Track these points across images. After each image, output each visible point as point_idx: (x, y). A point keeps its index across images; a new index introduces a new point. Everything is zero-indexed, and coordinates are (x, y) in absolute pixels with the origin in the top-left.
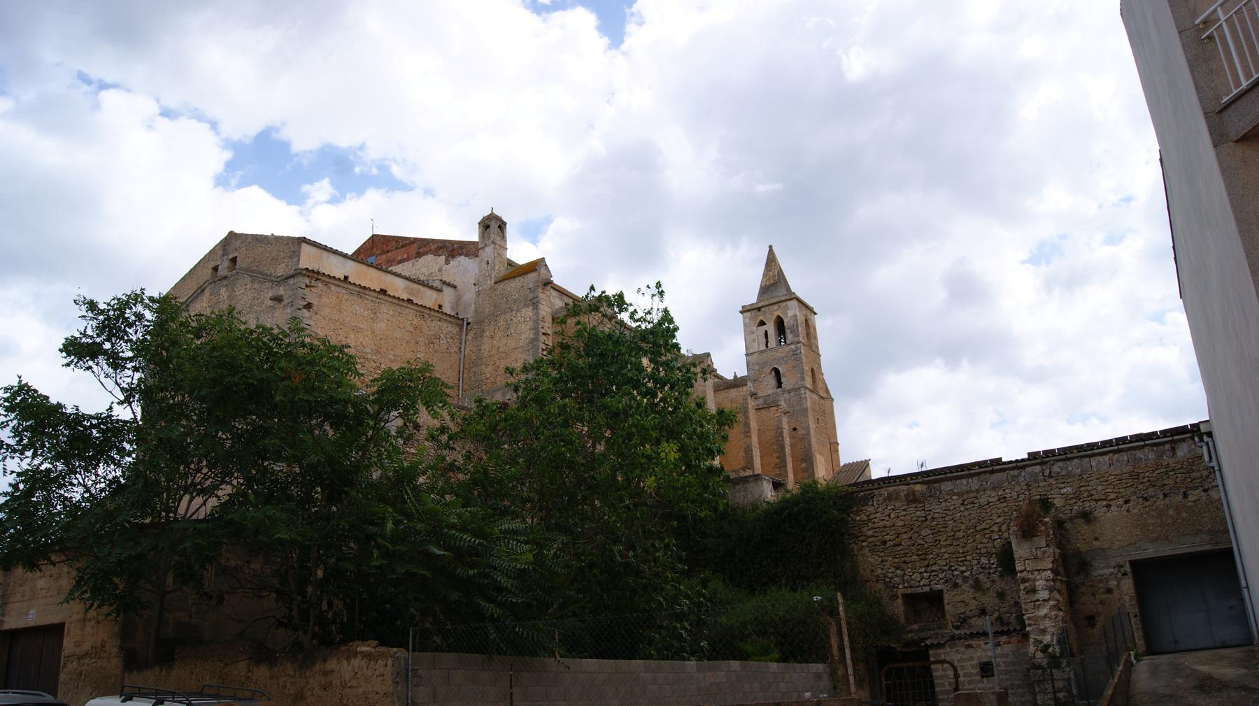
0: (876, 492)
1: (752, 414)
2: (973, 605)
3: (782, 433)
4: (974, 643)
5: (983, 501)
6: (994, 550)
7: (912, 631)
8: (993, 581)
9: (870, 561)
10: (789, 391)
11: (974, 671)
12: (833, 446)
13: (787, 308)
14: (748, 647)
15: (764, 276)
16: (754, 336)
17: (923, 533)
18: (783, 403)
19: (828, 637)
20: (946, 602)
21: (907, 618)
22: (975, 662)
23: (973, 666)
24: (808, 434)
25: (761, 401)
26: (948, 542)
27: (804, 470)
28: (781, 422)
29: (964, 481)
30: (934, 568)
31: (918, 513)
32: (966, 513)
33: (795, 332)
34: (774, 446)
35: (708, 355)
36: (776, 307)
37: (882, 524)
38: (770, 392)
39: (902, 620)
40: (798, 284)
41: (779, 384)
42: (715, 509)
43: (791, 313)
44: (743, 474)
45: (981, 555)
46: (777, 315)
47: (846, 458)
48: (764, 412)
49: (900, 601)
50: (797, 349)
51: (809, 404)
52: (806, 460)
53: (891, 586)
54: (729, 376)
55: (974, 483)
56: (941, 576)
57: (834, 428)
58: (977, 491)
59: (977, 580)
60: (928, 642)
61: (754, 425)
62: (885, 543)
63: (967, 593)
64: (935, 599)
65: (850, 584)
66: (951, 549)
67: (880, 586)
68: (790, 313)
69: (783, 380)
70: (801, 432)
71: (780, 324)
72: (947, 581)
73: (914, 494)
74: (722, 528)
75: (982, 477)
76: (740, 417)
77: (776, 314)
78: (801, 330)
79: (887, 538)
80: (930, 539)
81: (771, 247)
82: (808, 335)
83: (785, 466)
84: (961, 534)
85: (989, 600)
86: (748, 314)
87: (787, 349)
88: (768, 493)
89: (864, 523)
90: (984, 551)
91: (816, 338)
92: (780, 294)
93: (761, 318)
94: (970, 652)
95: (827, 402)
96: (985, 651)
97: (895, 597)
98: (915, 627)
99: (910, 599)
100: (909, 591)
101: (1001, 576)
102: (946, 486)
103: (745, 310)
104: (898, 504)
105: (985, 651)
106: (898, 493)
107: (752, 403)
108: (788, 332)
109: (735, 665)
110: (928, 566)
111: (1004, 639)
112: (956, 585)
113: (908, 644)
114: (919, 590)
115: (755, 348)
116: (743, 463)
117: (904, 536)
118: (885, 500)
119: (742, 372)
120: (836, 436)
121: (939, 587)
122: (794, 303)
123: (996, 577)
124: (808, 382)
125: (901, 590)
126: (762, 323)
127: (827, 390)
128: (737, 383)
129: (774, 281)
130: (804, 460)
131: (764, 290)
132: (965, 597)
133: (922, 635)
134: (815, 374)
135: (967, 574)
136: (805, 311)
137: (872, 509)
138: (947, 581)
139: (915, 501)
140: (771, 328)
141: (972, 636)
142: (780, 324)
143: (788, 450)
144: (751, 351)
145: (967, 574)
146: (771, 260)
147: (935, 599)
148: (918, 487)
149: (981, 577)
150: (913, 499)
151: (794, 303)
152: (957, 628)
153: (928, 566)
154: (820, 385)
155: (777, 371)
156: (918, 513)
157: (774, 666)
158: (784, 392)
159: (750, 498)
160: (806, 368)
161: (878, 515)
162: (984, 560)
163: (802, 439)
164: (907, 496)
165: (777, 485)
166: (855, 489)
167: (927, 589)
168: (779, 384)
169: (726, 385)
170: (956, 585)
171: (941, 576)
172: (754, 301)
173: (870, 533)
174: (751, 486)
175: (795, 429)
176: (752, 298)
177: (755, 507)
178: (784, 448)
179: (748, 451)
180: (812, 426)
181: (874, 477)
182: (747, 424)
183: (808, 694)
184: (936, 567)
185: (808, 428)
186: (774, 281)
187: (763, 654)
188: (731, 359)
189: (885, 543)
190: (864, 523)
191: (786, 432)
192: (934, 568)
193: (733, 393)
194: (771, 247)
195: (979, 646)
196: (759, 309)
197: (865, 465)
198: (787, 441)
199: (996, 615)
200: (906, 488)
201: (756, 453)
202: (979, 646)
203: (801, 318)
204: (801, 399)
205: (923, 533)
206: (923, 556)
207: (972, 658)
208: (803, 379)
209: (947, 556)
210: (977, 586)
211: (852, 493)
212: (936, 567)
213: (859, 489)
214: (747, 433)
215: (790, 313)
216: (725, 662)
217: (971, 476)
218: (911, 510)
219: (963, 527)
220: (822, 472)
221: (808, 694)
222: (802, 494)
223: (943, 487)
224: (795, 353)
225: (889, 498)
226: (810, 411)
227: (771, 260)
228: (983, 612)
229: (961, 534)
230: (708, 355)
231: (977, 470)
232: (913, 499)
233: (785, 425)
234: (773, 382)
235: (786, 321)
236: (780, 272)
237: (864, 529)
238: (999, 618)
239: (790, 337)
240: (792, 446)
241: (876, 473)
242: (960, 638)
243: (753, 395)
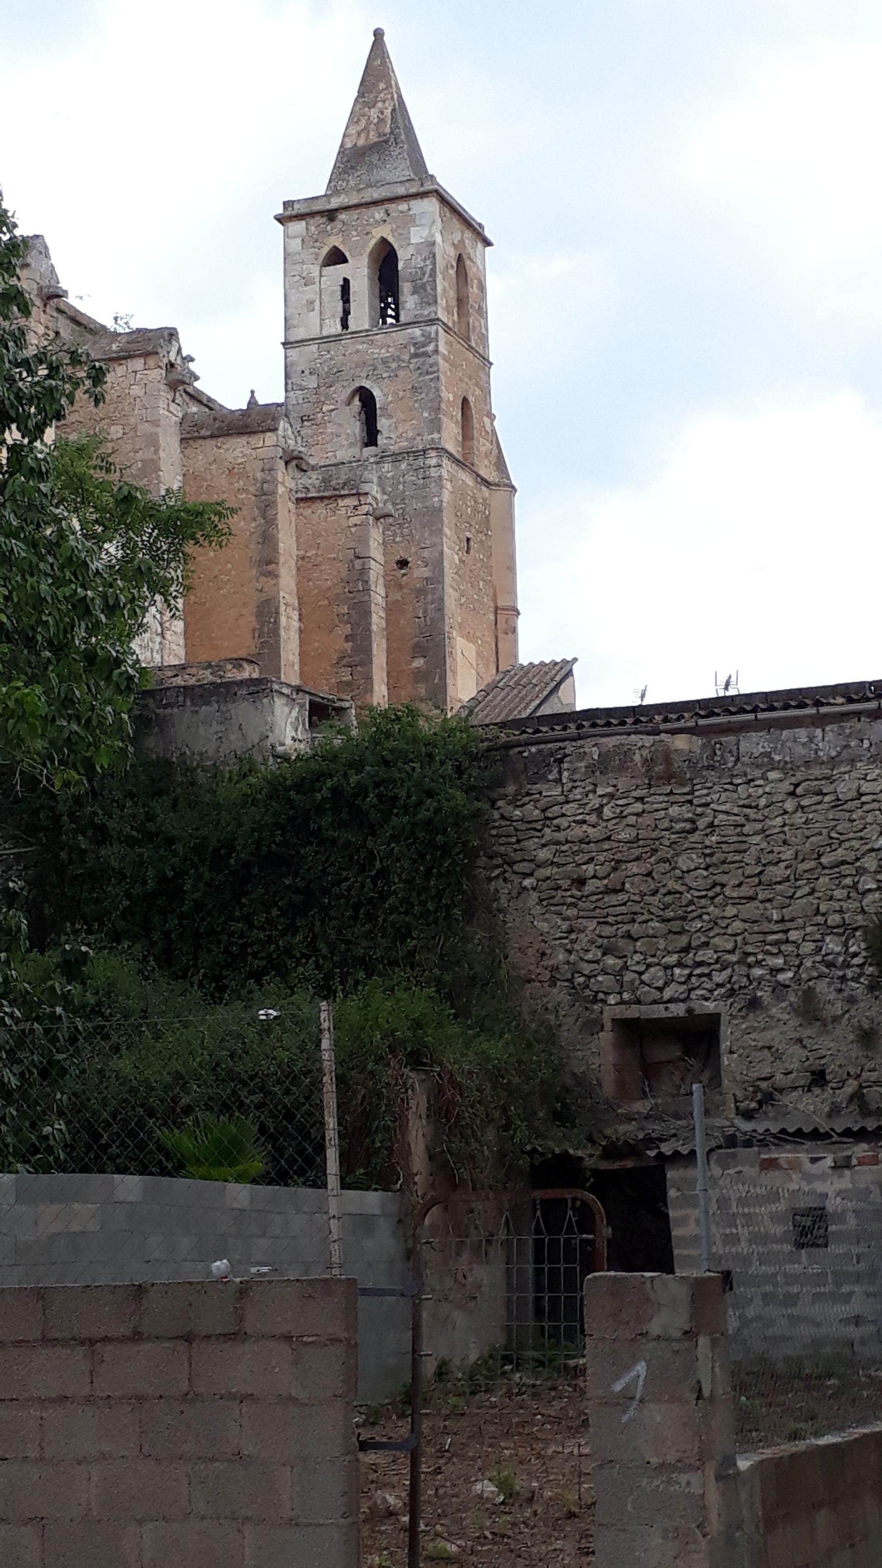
0: (569, 747)
1: (285, 511)
2: (794, 1058)
3: (364, 570)
4: (783, 1155)
5: (845, 788)
6: (860, 920)
7: (629, 1118)
8: (852, 1000)
9: (535, 929)
10: (397, 457)
11: (778, 1230)
12: (503, 618)
13: (409, 220)
14: (182, 1140)
15: (354, 119)
16: (311, 292)
17: (683, 863)
18: (374, 489)
19: (401, 1119)
20: (725, 1045)
21: (621, 1085)
22: (781, 1207)
23: (775, 1218)
24: (437, 579)
25: (313, 479)
26: (745, 891)
27: (420, 676)
28: (364, 540)
29: (802, 734)
30: (701, 956)
31: (674, 811)
32: (799, 818)
33: (425, 290)
34: (343, 607)
35: (171, 334)
36: (378, 213)
37: (578, 832)
38: (342, 455)
39: (608, 1088)
40: (449, 151)
41: (371, 436)
42: (89, 767)
43: (420, 234)
44: (232, 674)
45: (829, 929)
46: (382, 238)
47: (533, 647)
48: (320, 509)
49: (606, 1037)
50: (429, 339)
51: (446, 496)
52: (427, 649)
53: (587, 998)
54: (233, 400)
55: (827, 741)
56: (719, 977)
57: (511, 569)
58: (834, 762)
59: (809, 995)
60: (667, 1149)
61: (287, 543)
62: (581, 882)
63: (780, 1023)
64: (698, 1037)
65: (474, 988)
66: (751, 910)
67: (559, 994)
68: (417, 236)
69: (382, 423)
70: (419, 572)
71: (386, 262)
72: (732, 993)
73: (668, 761)
74: (151, 817)
75: (849, 726)
76: (242, 525)
77: (378, 233)
78: (444, 285)
79: (590, 869)
80: (699, 880)
81: (378, 34)
82: (461, 302)
83: (367, 661)
84: (778, 872)
85: (836, 1048)
86: (299, 227)
87: (401, 336)
88: (287, 728)
89: (532, 827)
90: (834, 919)
91: (482, 312)
92: (394, 174)
93: (336, 241)
94: (771, 1179)
95: (501, 494)
96: (808, 1178)
97: (593, 1026)
98: (641, 1107)
99: (633, 1032)
100: (633, 1012)
101: (871, 988)
102: (754, 744)
103: (290, 215)
104: (624, 782)
105: (808, 1178)
106: (627, 754)
107: (286, 482)
108: (406, 288)
109: (129, 1186)
110: (686, 950)
111: (861, 1150)
112: (754, 1004)
113: (612, 1151)
114: (659, 1012)
115: (310, 327)
116: (247, 646)
117: (634, 868)
118: (591, 769)
119: (272, 392)
120: (512, 592)
121: (710, 1006)
122: (431, 205)
123: (858, 988)
124: (450, 436)
125: (613, 1009)
126: (336, 257)
127: (500, 464)
128: (254, 421)
129: (380, 138)
130: (419, 650)
131: (351, 160)
132: (772, 1036)
133: (655, 1128)
134: (471, 413)
135: (786, 977)
136: (457, 233)
137: (557, 791)
138: (732, 993)
139: (669, 777)
140: (359, 272)
141: (783, 1137)
142: (386, 262)
143: (377, 620)
144: (300, 333)
145: (786, 977)
146: (377, 73)
147: (698, 1037)
148: (681, 742)
149: (821, 986)
150: (664, 773)
151: (431, 205)
152: (748, 1115)
153: (686, 950)
154: (482, 446)
155: (366, 399)
156: (674, 811)
157: (240, 1193)
158: (381, 459)
159: (235, 742)
160: (447, 396)
161: (572, 808)
162: (832, 945)
163: (420, 592)
164: (649, 762)
165: (320, 712)
166: (514, 735)
167: (678, 1010)
168: (371, 436)
169: (214, 425)
170: (754, 1004)
171: (719, 977)
172: (319, 188)
173: (543, 854)
174: (242, 710)
175: (403, 564)
176: (313, 181)
177: (247, 766)
178: (366, 614)
179: (267, 613)
180: (451, 556)
181: (581, 705)
182: (267, 539)
183: (220, 1265)
184: (707, 955)
185: (438, 564)
186: (380, 138)
187: (222, 1160)
188: (241, 358)
189: (581, 882)
190: (532, 827)
191: (376, 571)
192: (701, 956)
193: (237, 449)
194: (378, 34)
195: (795, 1165)
196: (331, 215)
197: (560, 673)
198: (378, 595)
199: (851, 1086)
200: (648, 740)
201: (289, 623)
202: (795, 1165)
203: (445, 253)
204: (426, 481)
205: (683, 863)
206: (676, 923)
207: (773, 1197)
208: (435, 425)
209: (737, 925)
210: (809, 1010)
211: (508, 746)
212: (707, 955)
213: (544, 733)
214: (267, 564)
215: (417, 236)
216: (96, 1179)
217: (820, 721)
218: (657, 801)
219: (788, 854)
220: (464, 685)
221: (220, 1265)
222: (375, 741)
223: (744, 746)
224: (421, 351)
225: (602, 766)
226: (447, 517)
227: (377, 73)
228: (819, 1078)
229: (778, 872)
230: (171, 334)
231: (839, 705)
232: (664, 773)
233: (375, 551)
234: (356, 429)
235: (403, 255)
236: (400, 110)
237: (530, 844)
238: (858, 1096)
239: (409, 302)
240: (391, 609)
241: (589, 694)
242: (748, 1144)
243: (294, 460)
